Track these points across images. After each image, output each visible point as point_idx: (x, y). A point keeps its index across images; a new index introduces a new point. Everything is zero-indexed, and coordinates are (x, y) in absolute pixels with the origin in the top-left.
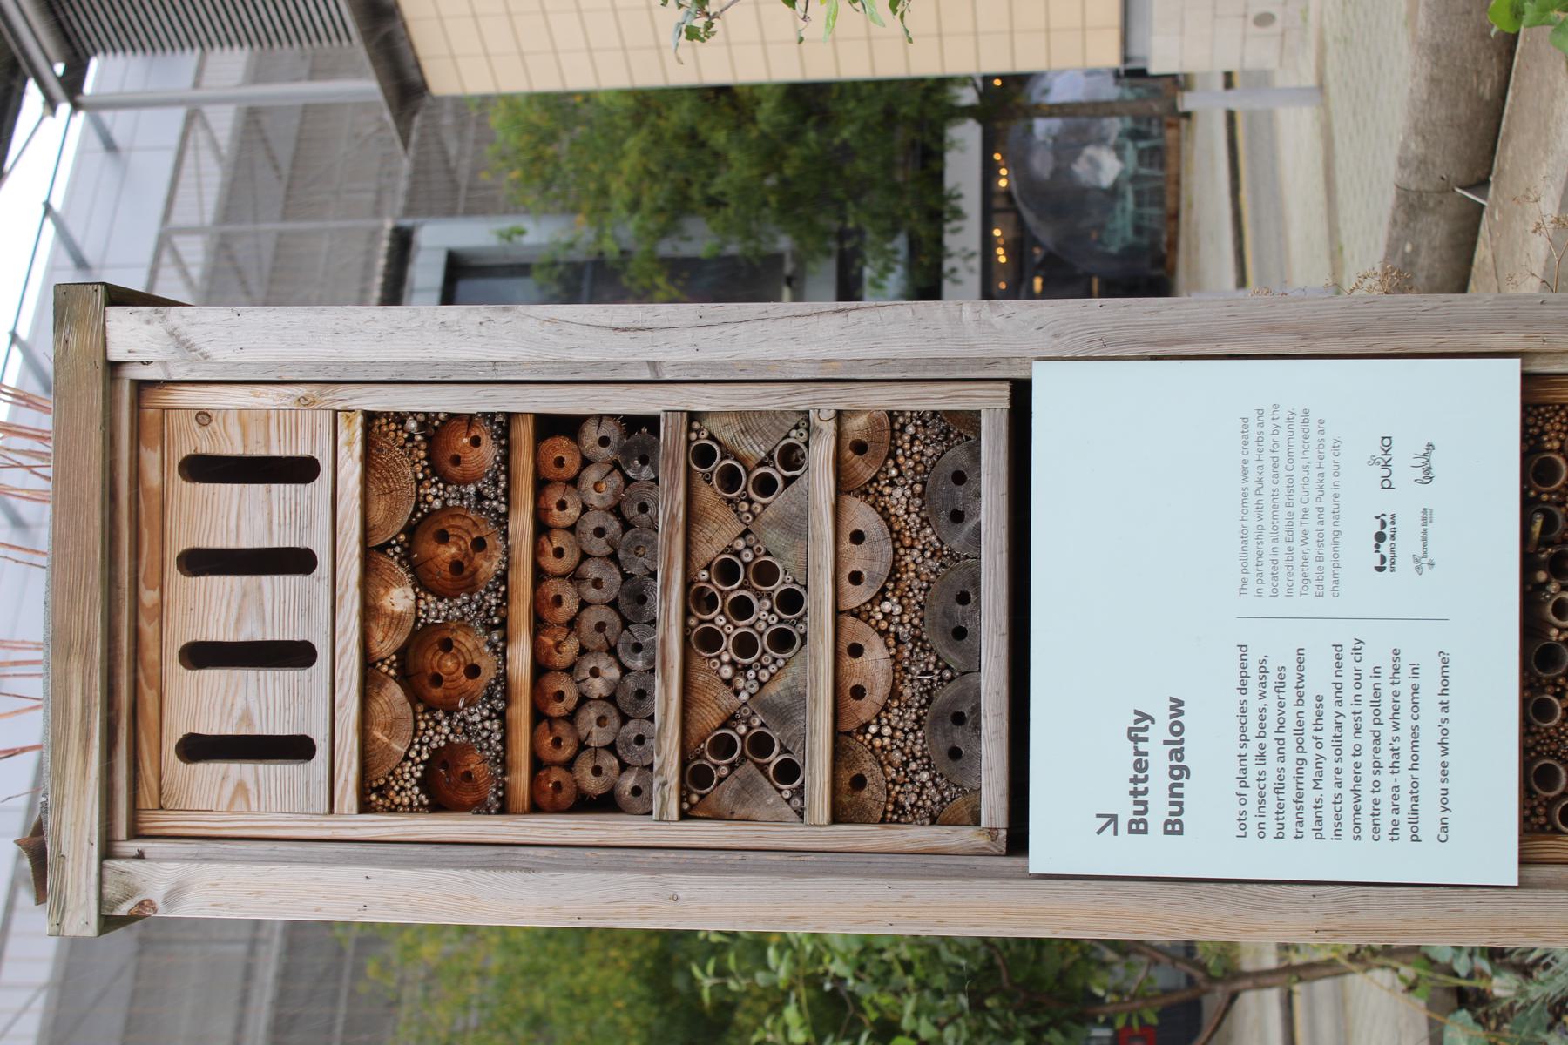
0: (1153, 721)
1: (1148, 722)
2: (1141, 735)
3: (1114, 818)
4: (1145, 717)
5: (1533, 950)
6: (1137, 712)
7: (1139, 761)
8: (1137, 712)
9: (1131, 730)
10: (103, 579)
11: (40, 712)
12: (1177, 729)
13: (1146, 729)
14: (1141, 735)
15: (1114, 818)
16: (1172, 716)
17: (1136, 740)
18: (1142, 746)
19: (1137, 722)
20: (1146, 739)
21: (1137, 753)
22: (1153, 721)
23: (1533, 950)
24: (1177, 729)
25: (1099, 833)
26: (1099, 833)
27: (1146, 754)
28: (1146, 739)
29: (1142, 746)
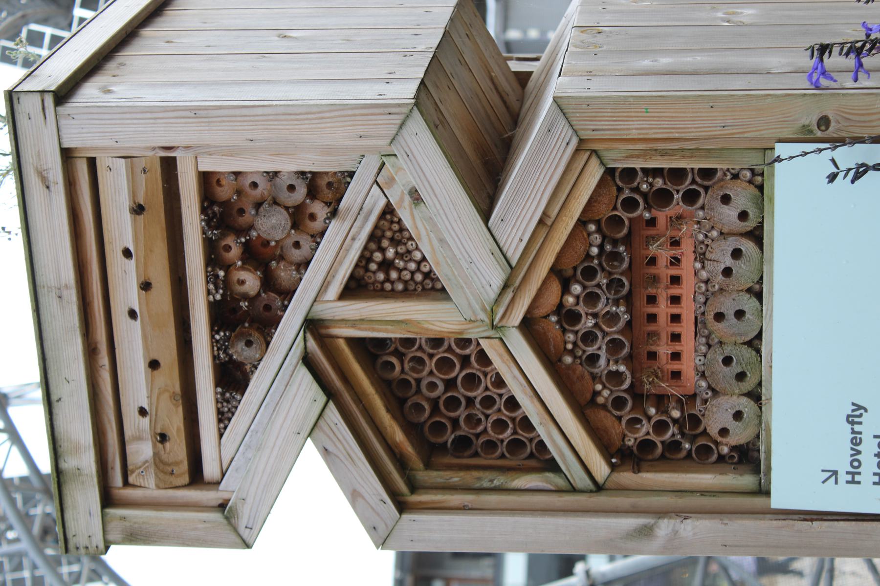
0: (866, 410)
1: (862, 411)
2: (856, 420)
3: (835, 473)
4: (860, 407)
5: (224, 418)
6: (853, 404)
7: (855, 438)
8: (853, 404)
9: (848, 416)
10: (615, 517)
11: (10, 157)
12: (856, 464)
13: (861, 416)
14: (856, 420)
15: (835, 473)
16: (852, 455)
17: (853, 423)
18: (857, 428)
19: (853, 411)
20: (860, 423)
21: (853, 432)
22: (866, 410)
23: (224, 418)
24: (856, 464)
25: (823, 482)
26: (823, 482)
27: (860, 433)
28: (860, 423)
29: (857, 428)
